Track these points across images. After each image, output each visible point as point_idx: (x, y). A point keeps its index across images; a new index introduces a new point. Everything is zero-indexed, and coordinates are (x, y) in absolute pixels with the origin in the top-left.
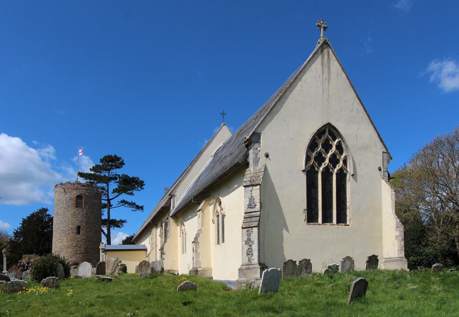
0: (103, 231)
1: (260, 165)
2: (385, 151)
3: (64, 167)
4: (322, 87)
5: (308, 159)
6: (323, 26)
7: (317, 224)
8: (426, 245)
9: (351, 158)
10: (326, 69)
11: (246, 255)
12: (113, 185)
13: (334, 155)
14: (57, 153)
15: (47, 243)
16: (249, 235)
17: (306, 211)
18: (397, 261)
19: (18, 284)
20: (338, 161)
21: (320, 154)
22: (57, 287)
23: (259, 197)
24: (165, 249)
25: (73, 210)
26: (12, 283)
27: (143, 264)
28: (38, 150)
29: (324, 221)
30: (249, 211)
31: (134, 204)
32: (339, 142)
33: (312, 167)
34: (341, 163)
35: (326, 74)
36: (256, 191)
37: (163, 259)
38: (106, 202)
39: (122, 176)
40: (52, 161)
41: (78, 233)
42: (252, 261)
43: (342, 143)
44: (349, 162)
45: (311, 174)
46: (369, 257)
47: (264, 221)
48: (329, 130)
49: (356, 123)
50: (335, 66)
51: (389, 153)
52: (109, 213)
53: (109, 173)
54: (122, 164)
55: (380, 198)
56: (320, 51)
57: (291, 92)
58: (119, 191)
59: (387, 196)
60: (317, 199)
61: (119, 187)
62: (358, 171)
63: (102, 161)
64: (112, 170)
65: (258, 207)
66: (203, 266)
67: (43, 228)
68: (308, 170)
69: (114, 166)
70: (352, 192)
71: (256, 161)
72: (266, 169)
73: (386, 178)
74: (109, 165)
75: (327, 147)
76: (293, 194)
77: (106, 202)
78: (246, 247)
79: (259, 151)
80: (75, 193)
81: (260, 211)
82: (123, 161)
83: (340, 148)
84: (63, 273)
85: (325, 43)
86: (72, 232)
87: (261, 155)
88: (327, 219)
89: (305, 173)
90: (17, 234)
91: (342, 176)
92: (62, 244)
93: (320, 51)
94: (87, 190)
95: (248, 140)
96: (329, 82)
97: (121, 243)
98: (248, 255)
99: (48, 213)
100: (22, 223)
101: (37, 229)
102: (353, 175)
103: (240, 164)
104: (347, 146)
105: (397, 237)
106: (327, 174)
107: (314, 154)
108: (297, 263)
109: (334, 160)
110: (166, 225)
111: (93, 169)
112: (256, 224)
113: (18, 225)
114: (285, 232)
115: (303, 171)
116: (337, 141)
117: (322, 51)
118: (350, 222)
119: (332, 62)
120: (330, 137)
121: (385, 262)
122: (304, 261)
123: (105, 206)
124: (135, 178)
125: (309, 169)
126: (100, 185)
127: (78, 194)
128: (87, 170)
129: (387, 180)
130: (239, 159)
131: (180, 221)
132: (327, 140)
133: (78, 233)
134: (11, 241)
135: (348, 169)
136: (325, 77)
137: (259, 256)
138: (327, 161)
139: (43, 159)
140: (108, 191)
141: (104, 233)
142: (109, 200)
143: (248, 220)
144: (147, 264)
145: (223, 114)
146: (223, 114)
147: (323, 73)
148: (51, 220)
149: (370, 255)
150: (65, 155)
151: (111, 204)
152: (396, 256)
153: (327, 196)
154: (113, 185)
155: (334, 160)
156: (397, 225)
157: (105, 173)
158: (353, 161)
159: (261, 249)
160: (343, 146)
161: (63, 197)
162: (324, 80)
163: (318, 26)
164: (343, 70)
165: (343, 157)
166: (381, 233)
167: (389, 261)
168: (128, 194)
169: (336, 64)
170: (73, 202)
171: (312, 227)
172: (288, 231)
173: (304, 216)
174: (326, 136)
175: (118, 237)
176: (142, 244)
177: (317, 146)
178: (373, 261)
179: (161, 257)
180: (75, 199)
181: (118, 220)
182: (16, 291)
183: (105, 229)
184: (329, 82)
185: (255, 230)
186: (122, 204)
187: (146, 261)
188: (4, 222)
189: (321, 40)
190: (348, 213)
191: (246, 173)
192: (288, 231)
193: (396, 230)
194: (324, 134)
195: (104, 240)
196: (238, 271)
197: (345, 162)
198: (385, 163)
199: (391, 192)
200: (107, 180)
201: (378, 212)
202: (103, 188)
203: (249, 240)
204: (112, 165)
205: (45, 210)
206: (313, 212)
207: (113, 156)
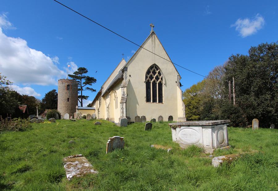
0: (79, 100)
1: (127, 80)
2: (178, 75)
3: (64, 68)
5: (146, 77)
6: (152, 26)
8: (212, 113)
10: (153, 43)
14: (60, 61)
15: (56, 105)
16: (122, 106)
17: (146, 98)
18: (182, 118)
19: (41, 120)
21: (151, 75)
22: (55, 122)
24: (99, 110)
25: (66, 91)
26: (38, 119)
28: (51, 58)
31: (92, 89)
32: (159, 71)
33: (148, 81)
34: (160, 79)
35: (153, 45)
36: (125, 89)
38: (80, 88)
40: (58, 65)
41: (68, 101)
43: (161, 72)
44: (163, 79)
45: (148, 84)
47: (128, 101)
50: (157, 41)
51: (180, 76)
52: (82, 93)
54: (87, 71)
56: (151, 36)
57: (138, 54)
58: (86, 83)
59: (179, 92)
60: (150, 93)
62: (167, 81)
63: (78, 70)
65: (126, 96)
66: (111, 117)
70: (165, 91)
71: (126, 78)
72: (129, 81)
73: (179, 86)
74: (81, 72)
75: (154, 73)
76: (140, 90)
77: (80, 88)
78: (122, 110)
80: (67, 84)
81: (127, 97)
83: (159, 73)
84: (58, 117)
85: (153, 32)
87: (128, 76)
88: (154, 101)
90: (43, 100)
91: (160, 85)
92: (61, 107)
93: (151, 36)
95: (122, 70)
96: (155, 48)
99: (56, 92)
102: (165, 84)
103: (120, 79)
104: (162, 73)
105: (183, 109)
106: (154, 84)
107: (149, 76)
108: (140, 117)
109: (157, 78)
110: (100, 99)
111: (75, 73)
112: (125, 102)
113: (43, 96)
114: (137, 105)
115: (145, 82)
116: (158, 71)
117: (152, 36)
119: (156, 40)
120: (156, 69)
121: (178, 119)
123: (80, 90)
126: (78, 80)
127: (68, 84)
128: (72, 74)
129: (179, 86)
130: (120, 77)
131: (105, 98)
132: (154, 70)
133: (68, 101)
134: (41, 104)
135: (163, 82)
137: (126, 114)
138: (154, 78)
139: (54, 62)
140: (81, 83)
141: (80, 101)
142: (82, 87)
143: (123, 100)
145: (123, 55)
146: (123, 55)
148: (57, 95)
150: (62, 65)
153: (154, 92)
154: (83, 81)
155: (157, 78)
157: (79, 75)
158: (165, 79)
159: (127, 111)
160: (161, 73)
161: (61, 85)
163: (150, 26)
164: (161, 43)
165: (161, 77)
167: (180, 119)
168: (89, 85)
169: (158, 40)
170: (66, 88)
171: (148, 104)
172: (138, 105)
173: (145, 99)
174: (153, 70)
175: (86, 103)
176: (94, 107)
178: (171, 118)
181: (86, 96)
182: (40, 122)
183: (80, 100)
184: (155, 48)
185: (125, 104)
188: (38, 93)
189: (151, 31)
192: (138, 105)
195: (79, 104)
196: (119, 119)
197: (162, 79)
198: (179, 80)
201: (176, 99)
202: (79, 82)
203: (123, 107)
204: (83, 72)
205: (55, 90)
206: (149, 98)
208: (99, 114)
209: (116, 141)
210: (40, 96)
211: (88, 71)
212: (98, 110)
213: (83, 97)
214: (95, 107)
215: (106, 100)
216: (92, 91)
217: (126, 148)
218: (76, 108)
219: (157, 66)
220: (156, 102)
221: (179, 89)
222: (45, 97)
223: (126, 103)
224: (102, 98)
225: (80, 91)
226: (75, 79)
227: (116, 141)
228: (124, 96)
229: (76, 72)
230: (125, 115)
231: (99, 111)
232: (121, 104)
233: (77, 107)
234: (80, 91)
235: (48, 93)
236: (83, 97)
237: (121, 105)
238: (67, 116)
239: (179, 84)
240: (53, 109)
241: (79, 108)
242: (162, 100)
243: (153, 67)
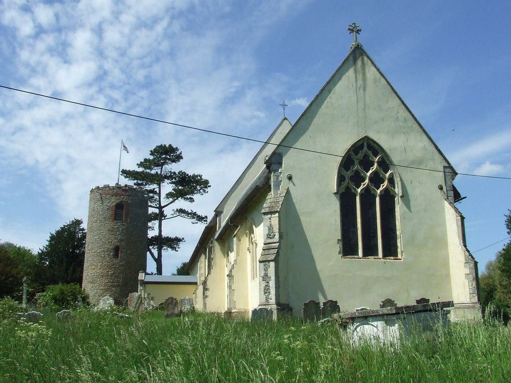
1: (282, 191)
4: (356, 96)
5: (341, 179)
7: (356, 257)
9: (398, 175)
10: (360, 77)
11: (263, 293)
12: (167, 187)
13: (376, 173)
16: (266, 270)
17: (341, 243)
18: (468, 308)
23: (278, 226)
25: (110, 224)
27: (170, 301)
29: (366, 254)
30: (268, 242)
31: (195, 214)
32: (382, 158)
33: (348, 188)
35: (360, 82)
37: (206, 297)
39: (179, 173)
42: (270, 301)
43: (385, 158)
45: (346, 199)
46: (305, 304)
47: (288, 258)
48: (368, 144)
49: (404, 133)
53: (161, 169)
54: (179, 158)
55: (443, 224)
63: (152, 153)
64: (166, 166)
65: (277, 236)
67: (75, 247)
69: (169, 159)
70: (403, 218)
72: (288, 192)
73: (451, 199)
75: (367, 165)
76: (322, 220)
77: (157, 211)
78: (264, 284)
79: (281, 173)
80: (114, 201)
82: (181, 154)
86: (109, 255)
87: (283, 178)
88: (370, 251)
89: (338, 195)
91: (388, 200)
93: (351, 58)
94: (129, 196)
96: (364, 90)
97: (176, 272)
98: (265, 293)
100: (49, 239)
101: (67, 245)
102: (401, 197)
103: (261, 188)
109: (376, 180)
112: (273, 257)
115: (335, 193)
118: (402, 255)
120: (370, 153)
122: (330, 303)
128: (133, 167)
129: (452, 201)
132: (366, 156)
133: (116, 255)
135: (396, 190)
142: (160, 208)
143: (267, 252)
144: (174, 301)
147: (356, 81)
151: (165, 213)
152: (468, 300)
154: (167, 187)
155: (376, 180)
156: (466, 260)
157: (155, 171)
159: (281, 285)
162: (358, 89)
165: (345, 184)
166: (448, 268)
168: (187, 199)
171: (348, 260)
173: (338, 248)
175: (173, 260)
177: (353, 163)
179: (204, 294)
180: (114, 208)
183: (155, 252)
184: (364, 90)
185: (272, 264)
187: (172, 298)
190: (399, 244)
191: (267, 198)
193: (465, 267)
195: (151, 266)
197: (391, 181)
198: (448, 178)
199: (456, 216)
200: (159, 179)
202: (153, 191)
203: (266, 275)
204: (165, 159)
207: (167, 146)
210: (35, 243)
211: (182, 158)
212: (205, 283)
213: (172, 243)
215: (252, 232)
218: (140, 278)
219: (375, 142)
220: (377, 254)
221: (452, 211)
222: (47, 243)
223: (276, 260)
224: (217, 247)
225: (157, 222)
226: (142, 184)
228: (271, 241)
229: (146, 160)
230: (273, 300)
232: (262, 264)
233: (141, 276)
234: (155, 224)
235: (58, 232)
236: (163, 242)
238: (106, 303)
239: (451, 193)
240: (68, 283)
241: (149, 279)
242: (396, 247)
243: (362, 146)
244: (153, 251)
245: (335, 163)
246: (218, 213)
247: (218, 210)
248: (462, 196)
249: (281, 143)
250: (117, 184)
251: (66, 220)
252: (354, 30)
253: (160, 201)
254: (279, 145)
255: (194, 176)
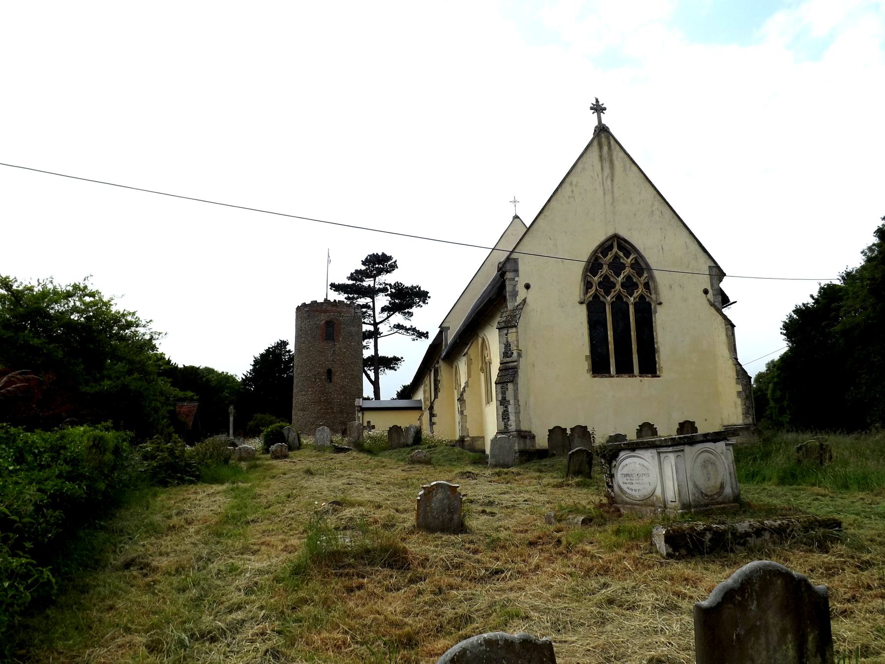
5: (588, 285)
10: (607, 165)
13: (629, 278)
20: (636, 286)
31: (414, 330)
35: (607, 171)
37: (434, 424)
43: (640, 260)
54: (394, 267)
58: (390, 309)
61: (390, 303)
68: (590, 302)
71: (515, 294)
73: (719, 305)
75: (617, 266)
77: (371, 328)
78: (502, 409)
87: (520, 288)
88: (625, 369)
89: (584, 307)
91: (646, 312)
97: (395, 397)
98: (503, 419)
105: (739, 393)
108: (569, 432)
111: (352, 277)
116: (631, 257)
119: (615, 153)
120: (621, 254)
124: (415, 288)
125: (591, 299)
126: (362, 301)
132: (616, 257)
136: (605, 175)
137: (518, 421)
140: (374, 310)
142: (375, 324)
149: (681, 421)
154: (382, 300)
155: (629, 285)
157: (368, 282)
165: (592, 292)
168: (405, 314)
173: (585, 365)
183: (372, 374)
186: (395, 330)
194: (611, 250)
195: (368, 390)
200: (371, 292)
202: (366, 306)
203: (504, 399)
208: (432, 424)
209: (440, 496)
212: (431, 408)
213: (391, 363)
214: (420, 396)
216: (414, 337)
217: (475, 522)
218: (356, 404)
222: (251, 368)
225: (372, 341)
227: (440, 496)
229: (357, 271)
231: (432, 415)
232: (499, 386)
235: (262, 355)
237: (499, 390)
239: (719, 298)
241: (367, 404)
243: (611, 248)
244: (369, 372)
245: (578, 269)
246: (443, 329)
247: (443, 326)
248: (731, 301)
249: (514, 249)
250: (326, 300)
251: (271, 342)
252: (598, 108)
253: (374, 316)
254: (512, 252)
255: (413, 288)
